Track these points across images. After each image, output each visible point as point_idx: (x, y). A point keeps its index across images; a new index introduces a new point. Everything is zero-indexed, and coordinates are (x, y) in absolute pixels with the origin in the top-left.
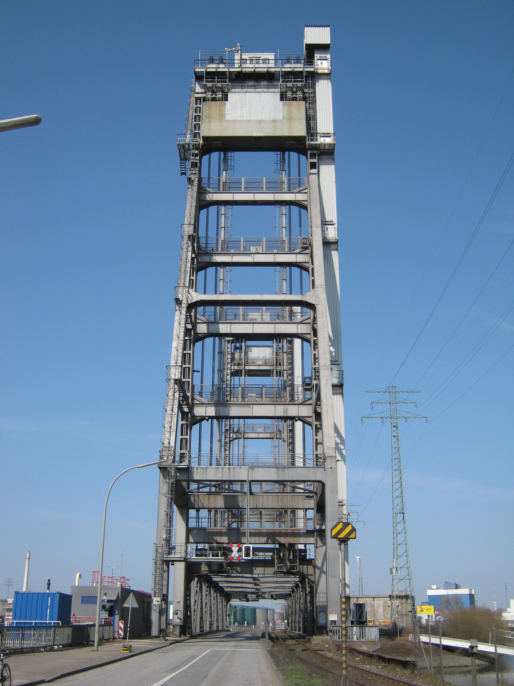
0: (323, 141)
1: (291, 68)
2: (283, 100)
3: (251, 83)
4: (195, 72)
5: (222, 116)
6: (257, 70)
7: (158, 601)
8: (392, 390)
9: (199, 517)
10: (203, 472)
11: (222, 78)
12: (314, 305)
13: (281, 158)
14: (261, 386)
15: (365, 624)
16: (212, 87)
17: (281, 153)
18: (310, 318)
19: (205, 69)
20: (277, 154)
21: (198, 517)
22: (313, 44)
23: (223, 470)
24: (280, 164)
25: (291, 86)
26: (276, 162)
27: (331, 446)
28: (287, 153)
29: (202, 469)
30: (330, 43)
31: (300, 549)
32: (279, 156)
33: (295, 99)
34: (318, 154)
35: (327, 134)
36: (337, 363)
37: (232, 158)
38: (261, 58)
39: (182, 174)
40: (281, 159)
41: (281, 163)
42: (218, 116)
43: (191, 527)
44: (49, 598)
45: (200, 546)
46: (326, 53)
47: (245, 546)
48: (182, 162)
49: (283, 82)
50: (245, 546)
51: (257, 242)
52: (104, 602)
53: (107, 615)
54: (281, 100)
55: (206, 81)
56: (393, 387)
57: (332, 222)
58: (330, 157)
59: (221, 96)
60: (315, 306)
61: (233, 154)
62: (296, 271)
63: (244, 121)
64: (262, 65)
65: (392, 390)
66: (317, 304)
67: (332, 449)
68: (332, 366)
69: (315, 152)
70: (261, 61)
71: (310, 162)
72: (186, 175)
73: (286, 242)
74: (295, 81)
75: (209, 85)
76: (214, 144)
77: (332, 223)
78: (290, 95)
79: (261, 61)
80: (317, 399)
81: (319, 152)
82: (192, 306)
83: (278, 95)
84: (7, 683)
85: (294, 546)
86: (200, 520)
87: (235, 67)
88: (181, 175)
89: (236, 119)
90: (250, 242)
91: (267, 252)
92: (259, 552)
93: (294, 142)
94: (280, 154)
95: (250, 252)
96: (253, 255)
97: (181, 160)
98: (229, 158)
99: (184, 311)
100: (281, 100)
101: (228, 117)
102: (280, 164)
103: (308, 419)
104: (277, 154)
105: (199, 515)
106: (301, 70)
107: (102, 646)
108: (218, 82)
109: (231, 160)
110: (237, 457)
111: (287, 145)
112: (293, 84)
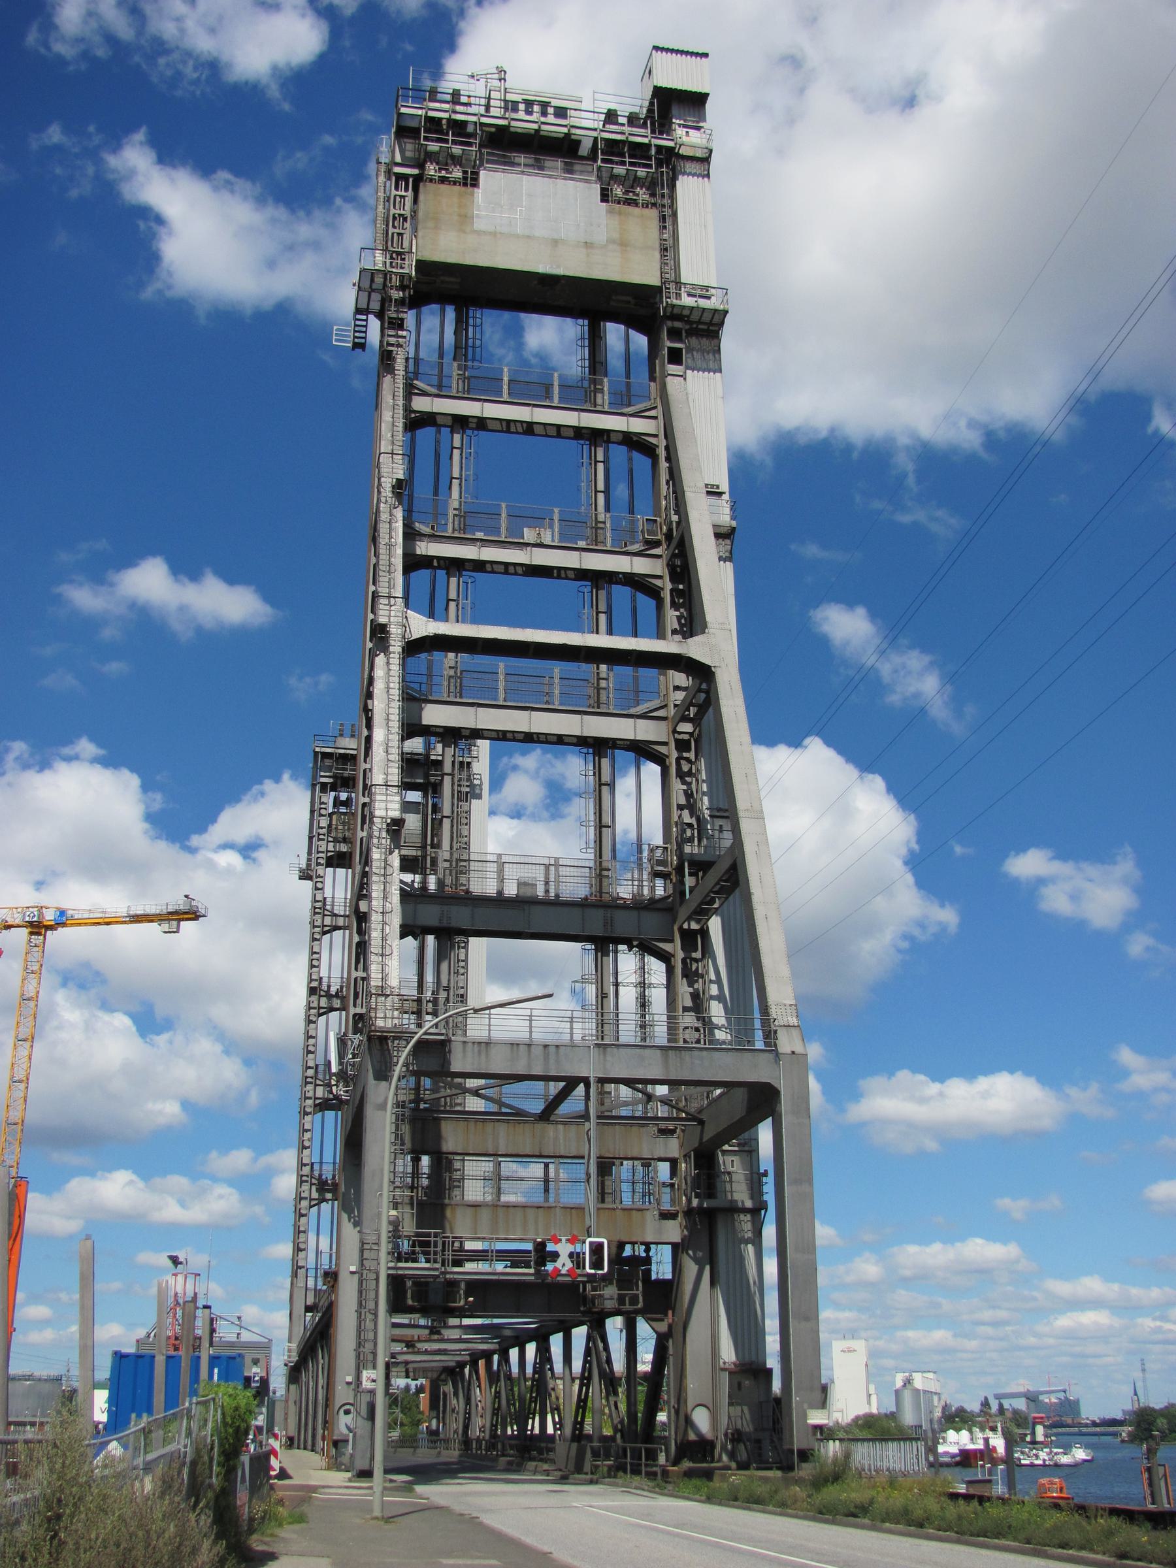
1: (623, 133)
2: (607, 201)
4: (400, 115)
5: (465, 218)
10: (479, 1052)
12: (710, 667)
14: (546, 862)
16: (438, 153)
18: (665, 706)
19: (424, 111)
22: (671, 89)
23: (529, 1051)
27: (785, 1002)
33: (632, 203)
36: (725, 814)
42: (456, 218)
44: (216, 1371)
48: (359, 317)
49: (603, 161)
51: (537, 520)
52: (254, 1381)
54: (602, 201)
55: (426, 139)
57: (718, 487)
58: (705, 342)
59: (460, 175)
62: (622, 593)
63: (517, 236)
69: (678, 324)
73: (608, 525)
74: (632, 164)
75: (433, 147)
76: (443, 282)
81: (687, 327)
82: (414, 647)
83: (596, 189)
87: (491, 114)
89: (499, 229)
90: (520, 518)
91: (563, 545)
93: (629, 298)
95: (521, 541)
96: (529, 548)
97: (358, 311)
98: (471, 321)
99: (395, 659)
100: (602, 201)
101: (479, 225)
106: (646, 141)
108: (454, 142)
111: (613, 303)
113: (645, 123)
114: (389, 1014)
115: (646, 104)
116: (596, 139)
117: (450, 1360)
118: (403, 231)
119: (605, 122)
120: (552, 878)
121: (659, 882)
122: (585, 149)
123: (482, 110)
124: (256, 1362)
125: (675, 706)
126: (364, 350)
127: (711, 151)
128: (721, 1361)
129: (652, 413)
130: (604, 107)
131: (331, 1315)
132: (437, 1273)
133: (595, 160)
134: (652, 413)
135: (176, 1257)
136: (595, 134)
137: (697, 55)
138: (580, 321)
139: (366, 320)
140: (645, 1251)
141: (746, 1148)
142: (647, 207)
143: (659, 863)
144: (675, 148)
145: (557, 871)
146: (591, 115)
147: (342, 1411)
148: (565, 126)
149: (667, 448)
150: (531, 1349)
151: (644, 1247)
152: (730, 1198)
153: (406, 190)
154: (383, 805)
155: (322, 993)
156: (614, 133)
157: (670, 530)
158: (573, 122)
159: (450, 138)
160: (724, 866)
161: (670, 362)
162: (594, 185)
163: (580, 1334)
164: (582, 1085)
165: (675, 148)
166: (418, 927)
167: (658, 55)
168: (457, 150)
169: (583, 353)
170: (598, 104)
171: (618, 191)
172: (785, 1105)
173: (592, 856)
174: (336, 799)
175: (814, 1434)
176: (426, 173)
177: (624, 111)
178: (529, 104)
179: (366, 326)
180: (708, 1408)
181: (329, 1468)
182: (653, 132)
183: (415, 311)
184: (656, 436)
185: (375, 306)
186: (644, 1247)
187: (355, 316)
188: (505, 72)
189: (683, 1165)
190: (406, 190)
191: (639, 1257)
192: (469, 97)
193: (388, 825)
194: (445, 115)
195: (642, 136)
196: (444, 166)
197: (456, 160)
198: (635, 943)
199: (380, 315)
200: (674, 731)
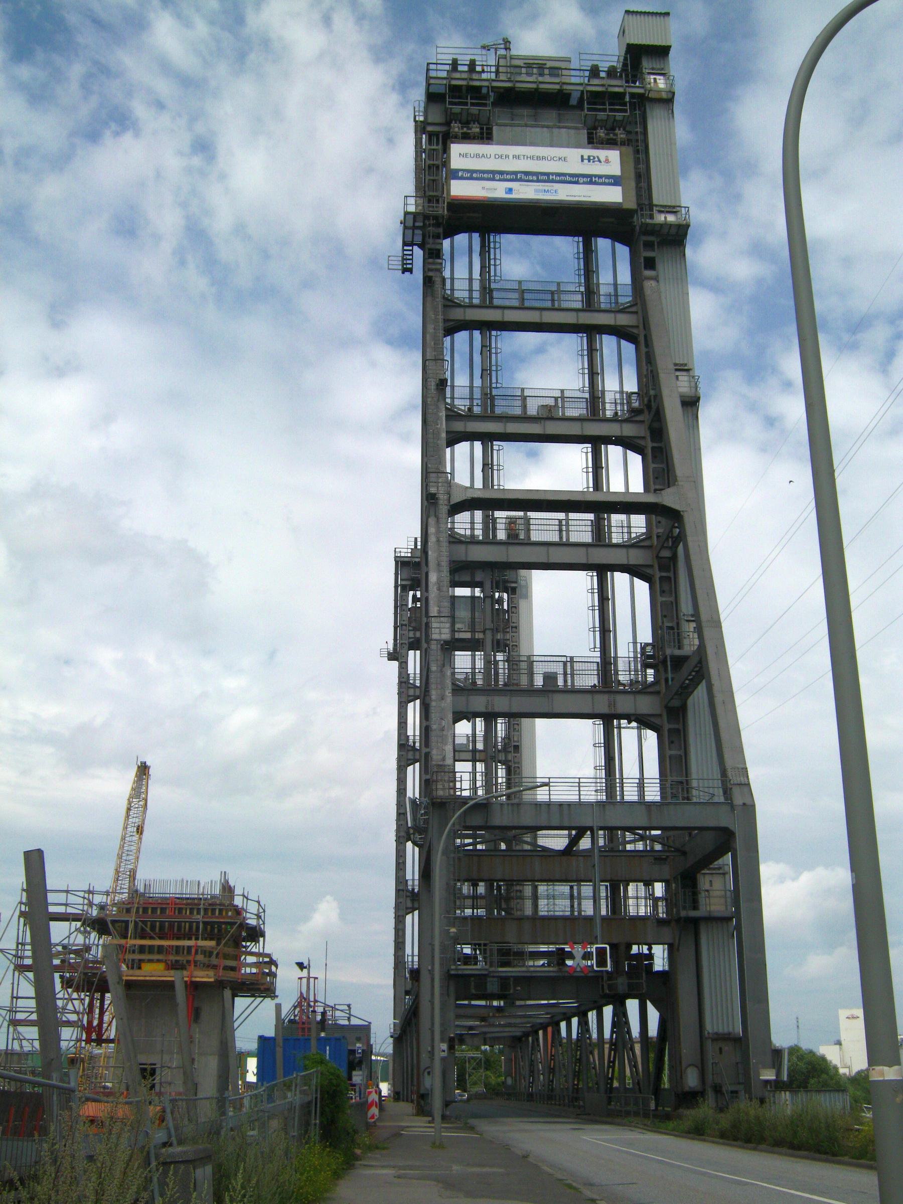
0: (663, 219)
3: (525, 112)
6: (542, 86)
14: (564, 659)
23: (549, 808)
25: (605, 118)
27: (738, 766)
29: (510, 806)
35: (670, 207)
38: (548, 66)
46: (662, 62)
47: (606, 948)
48: (406, 248)
49: (589, 110)
50: (606, 948)
55: (451, 103)
57: (686, 365)
59: (478, 130)
64: (547, 79)
66: (684, 509)
67: (740, 770)
70: (546, 71)
74: (611, 110)
75: (457, 109)
77: (686, 368)
78: (602, 135)
79: (535, 71)
84: (36, 1202)
88: (403, 273)
97: (405, 244)
98: (492, 245)
103: (653, 719)
106: (621, 90)
107: (705, 1143)
108: (472, 104)
110: (577, 784)
112: (608, 115)
113: (621, 76)
114: (446, 785)
115: (622, 59)
116: (582, 92)
117: (518, 1032)
118: (436, 178)
119: (590, 78)
120: (569, 671)
121: (650, 672)
122: (573, 101)
123: (493, 76)
124: (359, 1039)
125: (658, 537)
126: (411, 273)
127: (674, 94)
128: (706, 1032)
129: (634, 309)
130: (588, 65)
131: (418, 1003)
132: (486, 972)
133: (583, 110)
134: (634, 309)
135: (302, 963)
136: (581, 88)
137: (660, 14)
138: (576, 239)
139: (412, 250)
140: (648, 949)
141: (721, 871)
142: (624, 145)
143: (649, 657)
144: (645, 94)
145: (572, 667)
146: (577, 73)
147: (426, 1073)
148: (558, 83)
149: (645, 336)
150: (575, 1021)
151: (647, 947)
152: (708, 909)
153: (438, 144)
154: (437, 631)
155: (410, 748)
156: (596, 86)
157: (650, 401)
158: (565, 80)
159: (469, 101)
160: (694, 661)
161: (646, 268)
162: (582, 131)
163: (608, 1011)
164: (589, 833)
165: (645, 94)
166: (470, 713)
167: (631, 19)
168: (475, 110)
169: (579, 264)
170: (583, 63)
171: (601, 133)
172: (739, 844)
173: (598, 654)
174: (414, 596)
175: (766, 1086)
176: (451, 130)
177: (604, 66)
178: (529, 66)
179: (412, 255)
180: (696, 1067)
181: (417, 1114)
182: (627, 82)
183: (449, 239)
184: (637, 327)
185: (418, 239)
186: (647, 947)
187: (403, 247)
188: (510, 42)
189: (674, 885)
190: (437, 144)
191: (642, 954)
192: (483, 65)
193: (442, 645)
194: (464, 83)
195: (617, 86)
196: (466, 123)
197: (476, 119)
198: (632, 719)
199: (422, 246)
200: (657, 557)
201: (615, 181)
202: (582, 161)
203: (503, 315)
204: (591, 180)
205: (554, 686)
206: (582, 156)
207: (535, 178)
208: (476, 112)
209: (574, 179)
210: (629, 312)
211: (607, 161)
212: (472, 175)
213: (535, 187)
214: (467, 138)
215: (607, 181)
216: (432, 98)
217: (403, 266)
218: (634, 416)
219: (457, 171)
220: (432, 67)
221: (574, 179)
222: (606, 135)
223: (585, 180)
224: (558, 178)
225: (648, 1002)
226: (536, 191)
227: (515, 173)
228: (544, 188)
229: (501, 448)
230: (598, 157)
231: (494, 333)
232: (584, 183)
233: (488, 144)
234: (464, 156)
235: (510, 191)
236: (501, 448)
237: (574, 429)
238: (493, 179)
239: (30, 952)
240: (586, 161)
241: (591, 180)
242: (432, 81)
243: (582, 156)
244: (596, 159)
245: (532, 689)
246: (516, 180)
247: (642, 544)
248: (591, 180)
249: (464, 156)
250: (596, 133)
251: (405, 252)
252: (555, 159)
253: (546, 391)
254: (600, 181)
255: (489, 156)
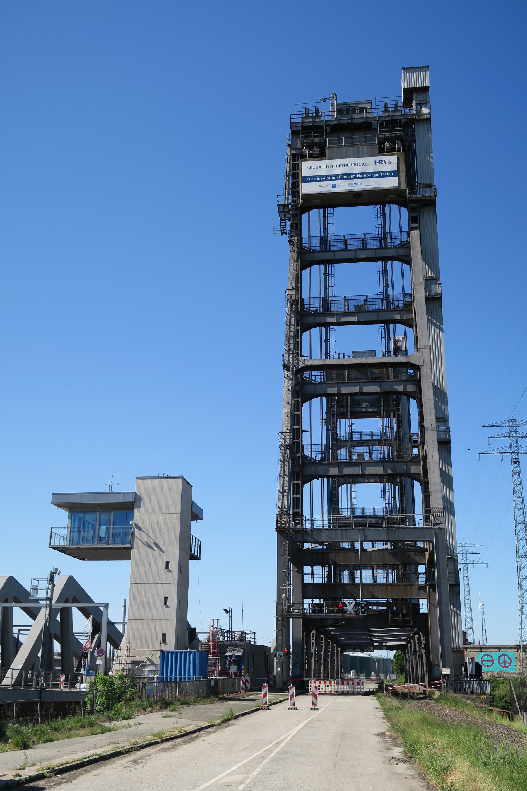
7: (281, 656)
8: (512, 424)
9: (313, 573)
11: (318, 133)
12: (419, 366)
13: (382, 212)
15: (481, 677)
17: (382, 206)
20: (378, 218)
21: (312, 574)
24: (381, 217)
26: (376, 217)
28: (387, 206)
30: (429, 86)
31: (412, 603)
32: (379, 209)
34: (419, 207)
37: (332, 215)
39: (282, 234)
40: (381, 213)
41: (382, 217)
43: (306, 583)
45: (316, 601)
48: (282, 222)
53: (236, 669)
56: (512, 420)
60: (420, 367)
61: (332, 210)
65: (512, 424)
66: (422, 365)
68: (439, 423)
71: (411, 207)
72: (286, 235)
80: (383, 659)
85: (407, 601)
86: (314, 575)
88: (282, 235)
92: (373, 606)
94: (381, 208)
97: (281, 220)
98: (329, 215)
102: (381, 217)
104: (378, 218)
105: (313, 571)
108: (315, 137)
109: (331, 216)
171: (388, 145)
201: (395, 173)
202: (375, 164)
203: (335, 256)
204: (314, 179)
205: (363, 460)
206: (375, 161)
207: (349, 177)
208: (318, 141)
209: (371, 175)
210: (403, 248)
211: (390, 162)
212: (314, 179)
213: (349, 182)
214: (312, 157)
215: (389, 174)
216: (295, 133)
217: (281, 232)
218: (406, 307)
219: (306, 177)
220: (292, 116)
221: (371, 175)
222: (390, 146)
223: (377, 175)
224: (362, 176)
225: (59, 621)
226: (350, 184)
227: (338, 175)
228: (353, 182)
229: (334, 330)
230: (384, 161)
231: (330, 265)
232: (376, 177)
233: (323, 160)
234: (310, 168)
235: (335, 186)
236: (334, 330)
237: (374, 317)
238: (326, 180)
239: (48, 601)
240: (377, 164)
241: (380, 175)
242: (293, 125)
243: (375, 161)
244: (384, 162)
245: (352, 461)
246: (338, 179)
247: (409, 379)
248: (314, 179)
249: (310, 168)
250: (384, 146)
251: (282, 224)
252: (360, 164)
253: (360, 296)
254: (386, 175)
255: (323, 167)
